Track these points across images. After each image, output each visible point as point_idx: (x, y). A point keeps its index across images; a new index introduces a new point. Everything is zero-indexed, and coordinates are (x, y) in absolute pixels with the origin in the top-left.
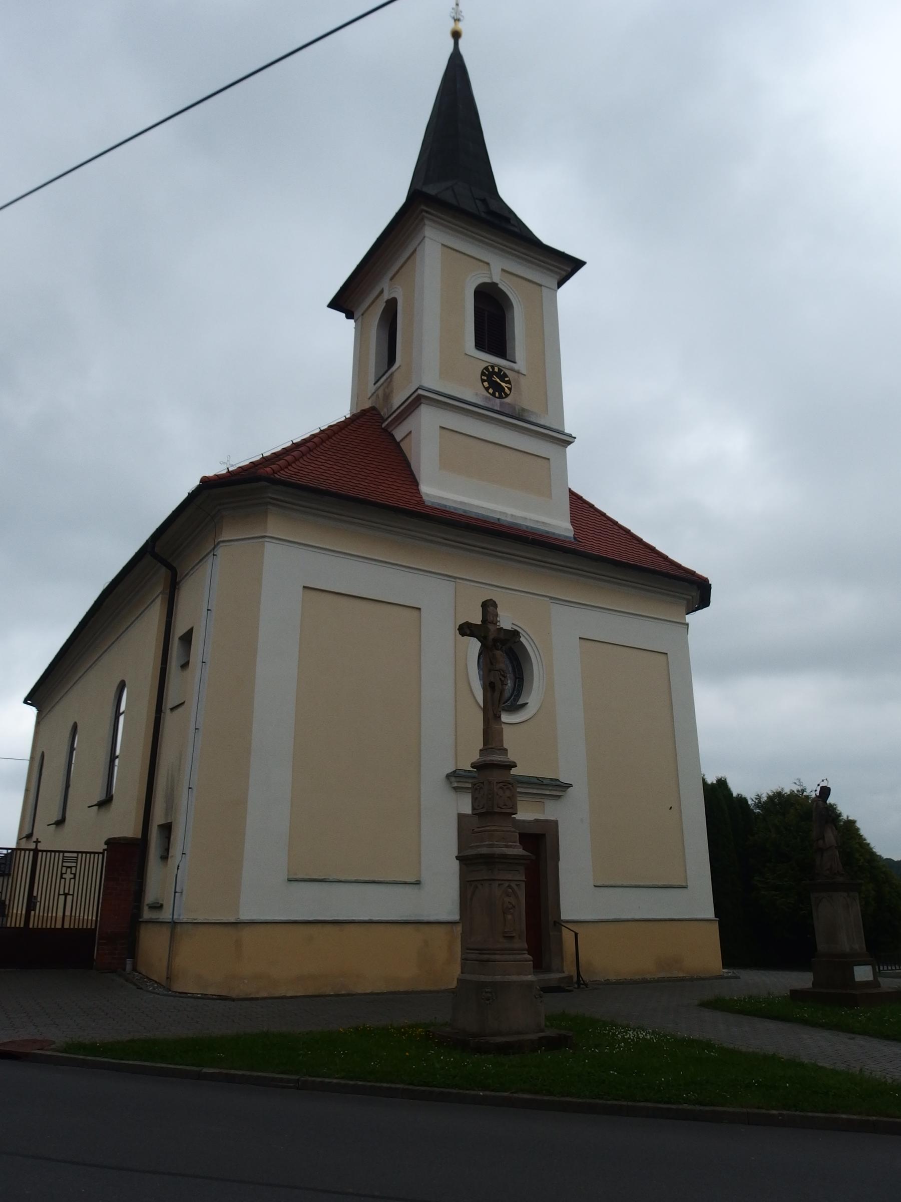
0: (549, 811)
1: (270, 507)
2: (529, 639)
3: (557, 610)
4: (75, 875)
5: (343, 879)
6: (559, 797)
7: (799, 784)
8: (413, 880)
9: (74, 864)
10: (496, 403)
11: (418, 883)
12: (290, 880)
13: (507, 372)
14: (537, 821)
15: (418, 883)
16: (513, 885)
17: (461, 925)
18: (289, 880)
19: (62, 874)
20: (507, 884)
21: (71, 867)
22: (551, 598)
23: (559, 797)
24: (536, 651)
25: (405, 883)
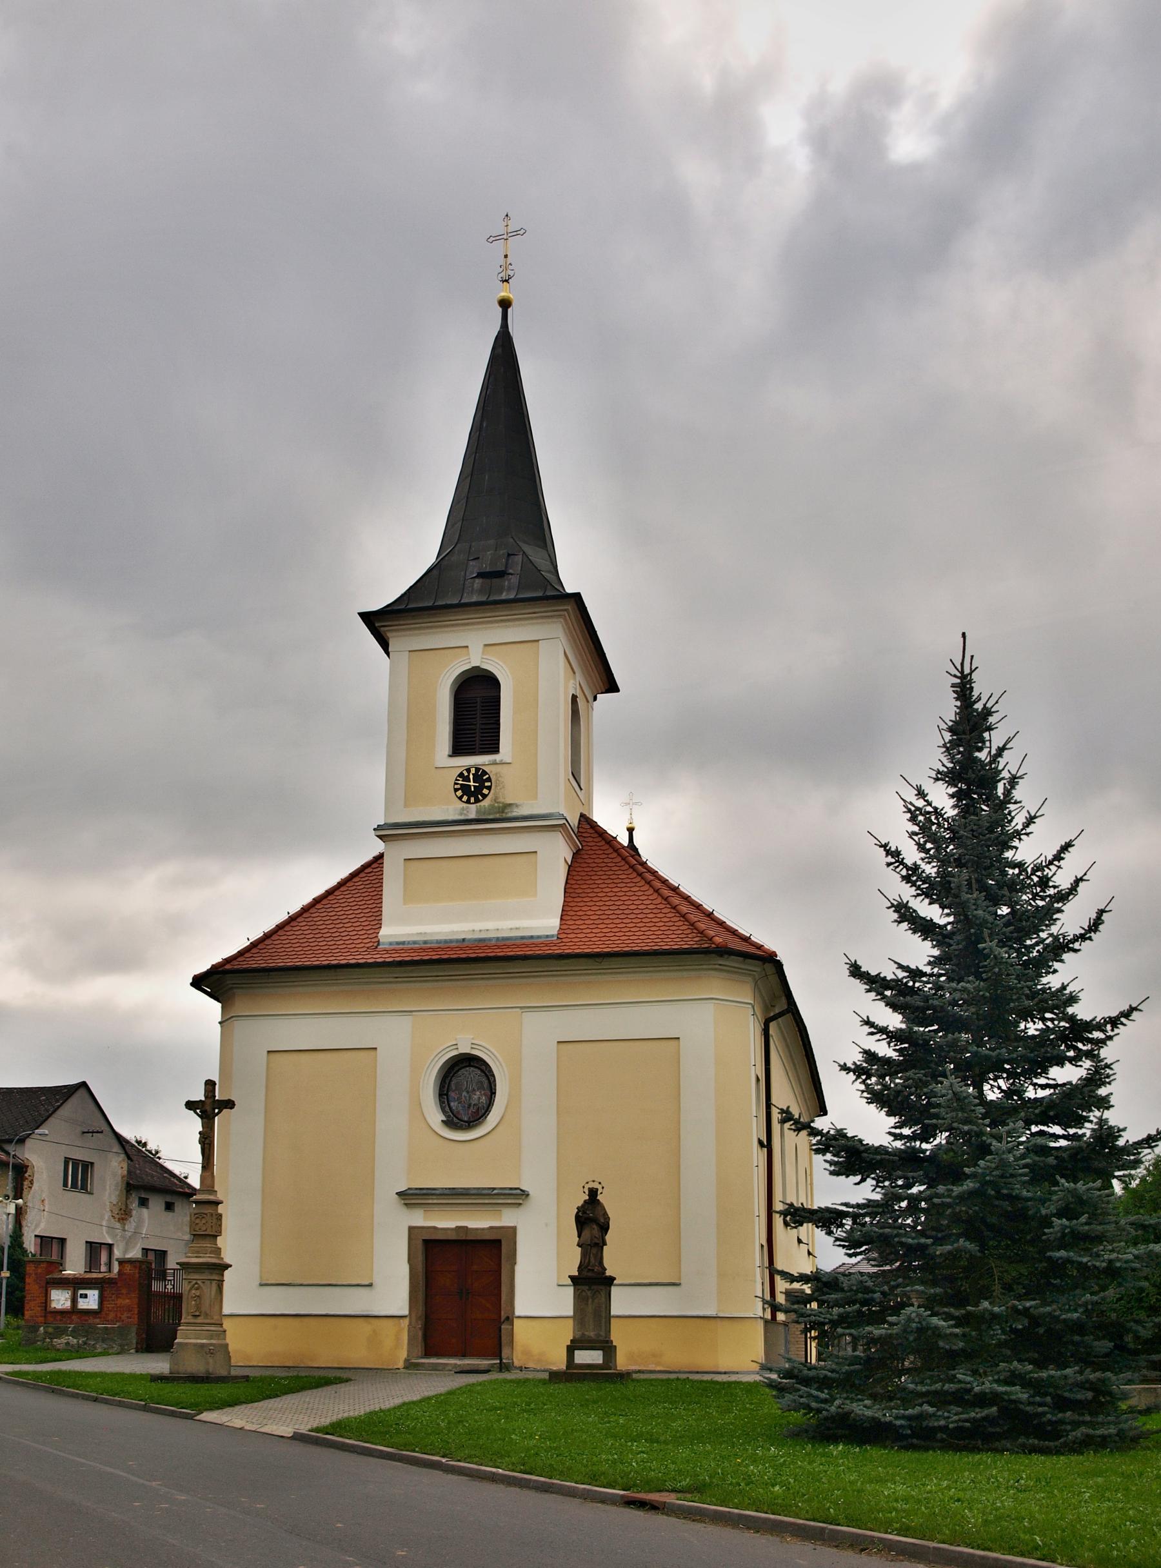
0: (506, 1218)
1: (235, 990)
2: (484, 1050)
3: (529, 1018)
4: (174, 1285)
5: (305, 1283)
6: (520, 1204)
7: (653, 1382)
8: (367, 1283)
9: (172, 1278)
10: (472, 811)
11: (370, 1285)
12: (261, 1285)
13: (486, 769)
14: (491, 1228)
15: (370, 1285)
16: (199, 1282)
17: (408, 1319)
18: (559, 1285)
19: (174, 1288)
20: (194, 1282)
21: (171, 1280)
22: (521, 1008)
23: (520, 1204)
24: (488, 1053)
25: (301, 1285)
